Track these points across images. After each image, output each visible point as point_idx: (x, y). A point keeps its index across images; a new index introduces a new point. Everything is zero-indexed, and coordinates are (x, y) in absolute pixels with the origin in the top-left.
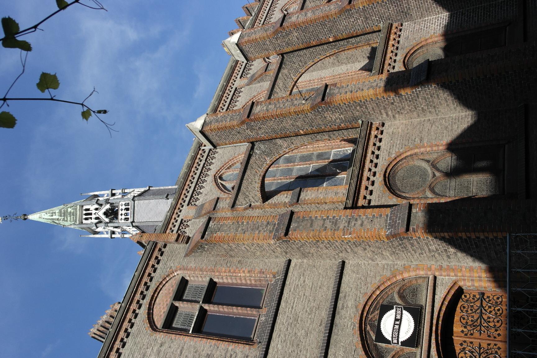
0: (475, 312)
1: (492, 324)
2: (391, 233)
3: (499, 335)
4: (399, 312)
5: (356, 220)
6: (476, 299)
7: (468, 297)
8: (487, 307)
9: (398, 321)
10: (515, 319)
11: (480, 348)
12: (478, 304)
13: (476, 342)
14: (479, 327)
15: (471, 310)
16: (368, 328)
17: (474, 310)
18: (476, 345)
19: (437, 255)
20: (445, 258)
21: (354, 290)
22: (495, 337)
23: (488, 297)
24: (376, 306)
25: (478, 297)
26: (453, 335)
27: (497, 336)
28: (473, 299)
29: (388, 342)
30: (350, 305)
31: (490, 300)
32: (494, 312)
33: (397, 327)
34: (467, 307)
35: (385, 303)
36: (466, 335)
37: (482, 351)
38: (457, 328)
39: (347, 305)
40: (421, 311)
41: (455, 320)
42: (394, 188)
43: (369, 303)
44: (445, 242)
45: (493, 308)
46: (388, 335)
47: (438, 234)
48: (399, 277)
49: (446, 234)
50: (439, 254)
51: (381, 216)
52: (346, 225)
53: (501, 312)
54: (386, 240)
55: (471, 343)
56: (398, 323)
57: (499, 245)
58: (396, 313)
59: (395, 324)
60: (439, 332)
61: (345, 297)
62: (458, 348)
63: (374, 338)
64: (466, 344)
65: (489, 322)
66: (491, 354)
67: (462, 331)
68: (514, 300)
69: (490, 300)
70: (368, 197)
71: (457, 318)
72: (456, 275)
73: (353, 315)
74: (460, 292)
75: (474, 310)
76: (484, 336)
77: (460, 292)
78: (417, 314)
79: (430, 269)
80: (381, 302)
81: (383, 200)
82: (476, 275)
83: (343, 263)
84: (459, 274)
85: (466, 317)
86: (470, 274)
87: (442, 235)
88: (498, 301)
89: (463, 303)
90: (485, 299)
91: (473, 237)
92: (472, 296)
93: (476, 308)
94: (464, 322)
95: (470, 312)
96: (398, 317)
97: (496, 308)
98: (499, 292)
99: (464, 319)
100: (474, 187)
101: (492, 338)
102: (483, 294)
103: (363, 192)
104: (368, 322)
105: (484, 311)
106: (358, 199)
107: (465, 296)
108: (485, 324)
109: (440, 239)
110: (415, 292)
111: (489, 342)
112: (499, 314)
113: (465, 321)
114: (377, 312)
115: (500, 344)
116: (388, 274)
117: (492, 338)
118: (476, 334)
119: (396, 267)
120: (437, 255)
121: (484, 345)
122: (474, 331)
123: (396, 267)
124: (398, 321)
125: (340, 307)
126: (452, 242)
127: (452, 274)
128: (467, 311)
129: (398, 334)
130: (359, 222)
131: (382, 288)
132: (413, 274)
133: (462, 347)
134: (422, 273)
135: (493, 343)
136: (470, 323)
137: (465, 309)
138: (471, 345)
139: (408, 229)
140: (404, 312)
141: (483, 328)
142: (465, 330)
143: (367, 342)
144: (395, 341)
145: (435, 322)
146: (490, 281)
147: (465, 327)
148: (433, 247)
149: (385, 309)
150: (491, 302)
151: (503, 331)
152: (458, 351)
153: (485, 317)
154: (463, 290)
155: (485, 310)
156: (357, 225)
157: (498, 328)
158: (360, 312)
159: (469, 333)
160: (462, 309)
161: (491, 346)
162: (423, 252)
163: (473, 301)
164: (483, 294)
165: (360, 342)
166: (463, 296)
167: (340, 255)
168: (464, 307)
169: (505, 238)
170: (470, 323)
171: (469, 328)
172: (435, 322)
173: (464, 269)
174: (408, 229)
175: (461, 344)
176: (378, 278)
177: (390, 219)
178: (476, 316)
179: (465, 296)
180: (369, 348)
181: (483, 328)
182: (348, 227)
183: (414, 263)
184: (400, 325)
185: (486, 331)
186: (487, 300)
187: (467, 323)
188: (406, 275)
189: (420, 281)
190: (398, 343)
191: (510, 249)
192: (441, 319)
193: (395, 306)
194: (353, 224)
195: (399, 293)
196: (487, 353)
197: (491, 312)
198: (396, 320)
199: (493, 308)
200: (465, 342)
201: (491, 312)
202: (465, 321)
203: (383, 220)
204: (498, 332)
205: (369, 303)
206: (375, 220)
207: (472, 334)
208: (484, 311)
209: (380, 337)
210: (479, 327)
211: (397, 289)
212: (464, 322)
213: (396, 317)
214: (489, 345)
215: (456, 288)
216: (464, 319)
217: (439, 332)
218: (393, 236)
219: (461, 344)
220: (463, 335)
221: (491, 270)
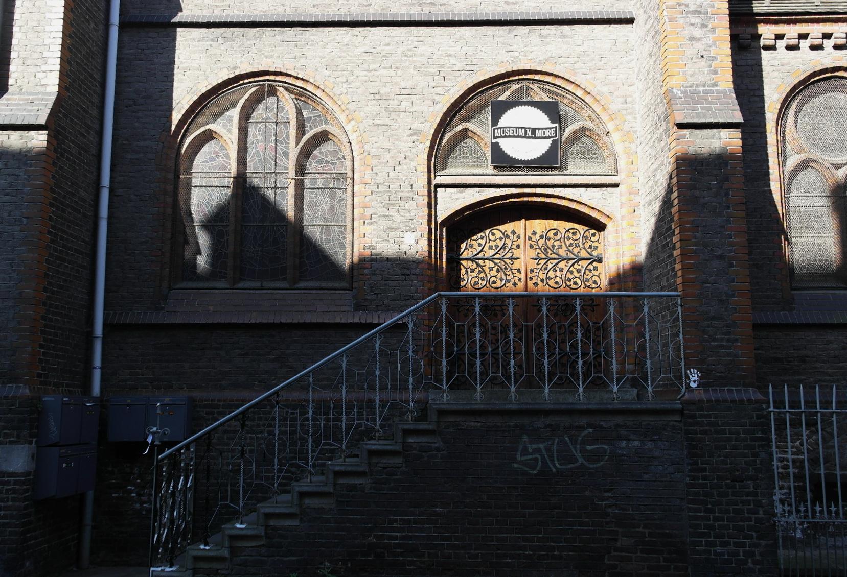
0: (569, 250)
1: (551, 274)
2: (675, 97)
3: (536, 284)
4: (547, 134)
5: (704, 26)
6: (589, 250)
7: (593, 239)
8: (578, 267)
9: (533, 133)
10: (562, 304)
11: (511, 259)
12: (583, 254)
13: (519, 253)
14: (544, 256)
15: (571, 245)
16: (515, 87)
17: (571, 248)
18: (517, 253)
19: (651, 183)
20: (647, 199)
21: (579, 49)
22: (531, 279)
23: (596, 269)
24: (557, 94)
25: (595, 253)
26: (527, 219)
27: (534, 280)
28: (590, 247)
29: (495, 121)
30: (549, 48)
31: (590, 271)
32: (571, 276)
33: (522, 133)
34: (575, 238)
35: (561, 107)
36: (530, 239)
37: (508, 261)
38: (539, 225)
39: (548, 43)
40: (556, 168)
41: (552, 221)
42: (807, 92)
43: (558, 82)
44: (667, 193)
45: (578, 275)
46: (511, 118)
47: (675, 180)
48: (610, 126)
49: (675, 194)
50: (652, 187)
51: (715, 73)
52: (692, 8)
53: (573, 286)
54: (664, 89)
55: (518, 246)
56: (529, 133)
57: (668, 280)
58: (546, 129)
59: (526, 129)
60: (526, 199)
61: (564, 36)
62: (508, 227)
63: (500, 99)
64: (515, 239)
65: (555, 270)
66: (506, 275)
67: (534, 233)
68: (593, 303)
69: (590, 271)
70: (781, 44)
71: (555, 224)
72: (623, 218)
73: (531, 56)
74: (599, 227)
75: (571, 248)
76: (532, 264)
77: (599, 227)
78: (550, 162)
79: (630, 174)
80: (566, 101)
81: (776, 74)
82: (626, 248)
83: (631, 21)
84: (625, 224)
85: (559, 236)
86: (627, 238)
87: (675, 189)
88: (591, 282)
89: (582, 233)
90: (591, 263)
91: (675, 239)
92: (594, 244)
93: (575, 251)
94: (551, 234)
95: (568, 243)
96: (538, 133)
97: (578, 281)
98: (604, 282)
99: (556, 234)
100: (810, 239)
101: (529, 275)
102: (600, 261)
103: (792, 31)
104: (524, 83)
105: (571, 262)
106: (776, 22)
107: (594, 235)
108: (550, 266)
109: (669, 185)
110: (588, 155)
111: (523, 271)
112: (569, 284)
113: (552, 236)
114: (546, 98)
115: (521, 285)
116: (613, 107)
117: (529, 275)
118: (532, 253)
119: (629, 118)
120: (651, 183)
121: (517, 264)
122: (538, 251)
123: (629, 118)
124: (533, 133)
125: (543, 32)
126: (667, 203)
127: (624, 211)
128: (568, 238)
129: (510, 136)
130: (698, 32)
131: (588, 99)
132: (619, 148)
133: (509, 233)
134: (622, 164)
135: (522, 276)
136: (549, 243)
137: (571, 235)
138: (514, 247)
139: (681, 126)
140: (549, 141)
141: (543, 262)
142: (538, 237)
143: (491, 88)
144: (497, 133)
145: (539, 190)
146: (618, 269)
147: (542, 237)
148: (659, 176)
149: (550, 109)
150: (587, 272)
151: (543, 289)
152: (502, 228)
153: (562, 265)
154: (604, 230)
155: (573, 265)
156: (692, 28)
157: (547, 283)
158: (539, 69)
159: (533, 243)
160: (572, 231)
161: (517, 274)
162: (653, 160)
163: (587, 246)
164: (600, 261)
165: (487, 77)
166: (593, 231)
167: (642, 11)
168: (574, 234)
169: (676, 290)
170: (549, 243)
171: (541, 242)
172: (539, 190)
173: (634, 229)
174: (681, 126)
175: (514, 232)
176: (605, 89)
177: (706, 92)
178: (562, 252)
179: (594, 235)
180: (482, 92)
181: (543, 262)
182: (688, 13)
183: (639, 150)
184: (526, 137)
185: (540, 266)
186: (590, 267)
187: (550, 239)
188: (615, 137)
189: (610, 162)
190: (495, 138)
191: (650, 296)
192: (548, 200)
193: (556, 125)
194: (693, 21)
195: (584, 129)
196: (506, 269)
197: (572, 272)
198: (533, 130)
199: (578, 275)
200: (519, 237)
201: (572, 272)
202: (552, 236)
203: (706, 78)
204: (539, 282)
205: (558, 82)
206: (703, 63)
207: (531, 246)
208: (571, 262)
209: (499, 109)
210: (544, 256)
211: (589, 125)
212: (551, 234)
213: (539, 129)
214: (519, 271)
215: (603, 220)
216: (556, 234)
217: (526, 199)
218: (669, 99)
219: (514, 232)
220: (529, 234)
221: (636, 270)
